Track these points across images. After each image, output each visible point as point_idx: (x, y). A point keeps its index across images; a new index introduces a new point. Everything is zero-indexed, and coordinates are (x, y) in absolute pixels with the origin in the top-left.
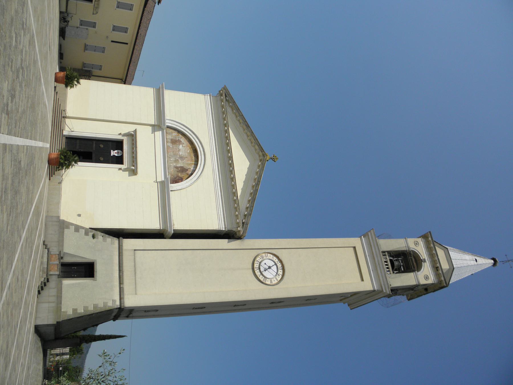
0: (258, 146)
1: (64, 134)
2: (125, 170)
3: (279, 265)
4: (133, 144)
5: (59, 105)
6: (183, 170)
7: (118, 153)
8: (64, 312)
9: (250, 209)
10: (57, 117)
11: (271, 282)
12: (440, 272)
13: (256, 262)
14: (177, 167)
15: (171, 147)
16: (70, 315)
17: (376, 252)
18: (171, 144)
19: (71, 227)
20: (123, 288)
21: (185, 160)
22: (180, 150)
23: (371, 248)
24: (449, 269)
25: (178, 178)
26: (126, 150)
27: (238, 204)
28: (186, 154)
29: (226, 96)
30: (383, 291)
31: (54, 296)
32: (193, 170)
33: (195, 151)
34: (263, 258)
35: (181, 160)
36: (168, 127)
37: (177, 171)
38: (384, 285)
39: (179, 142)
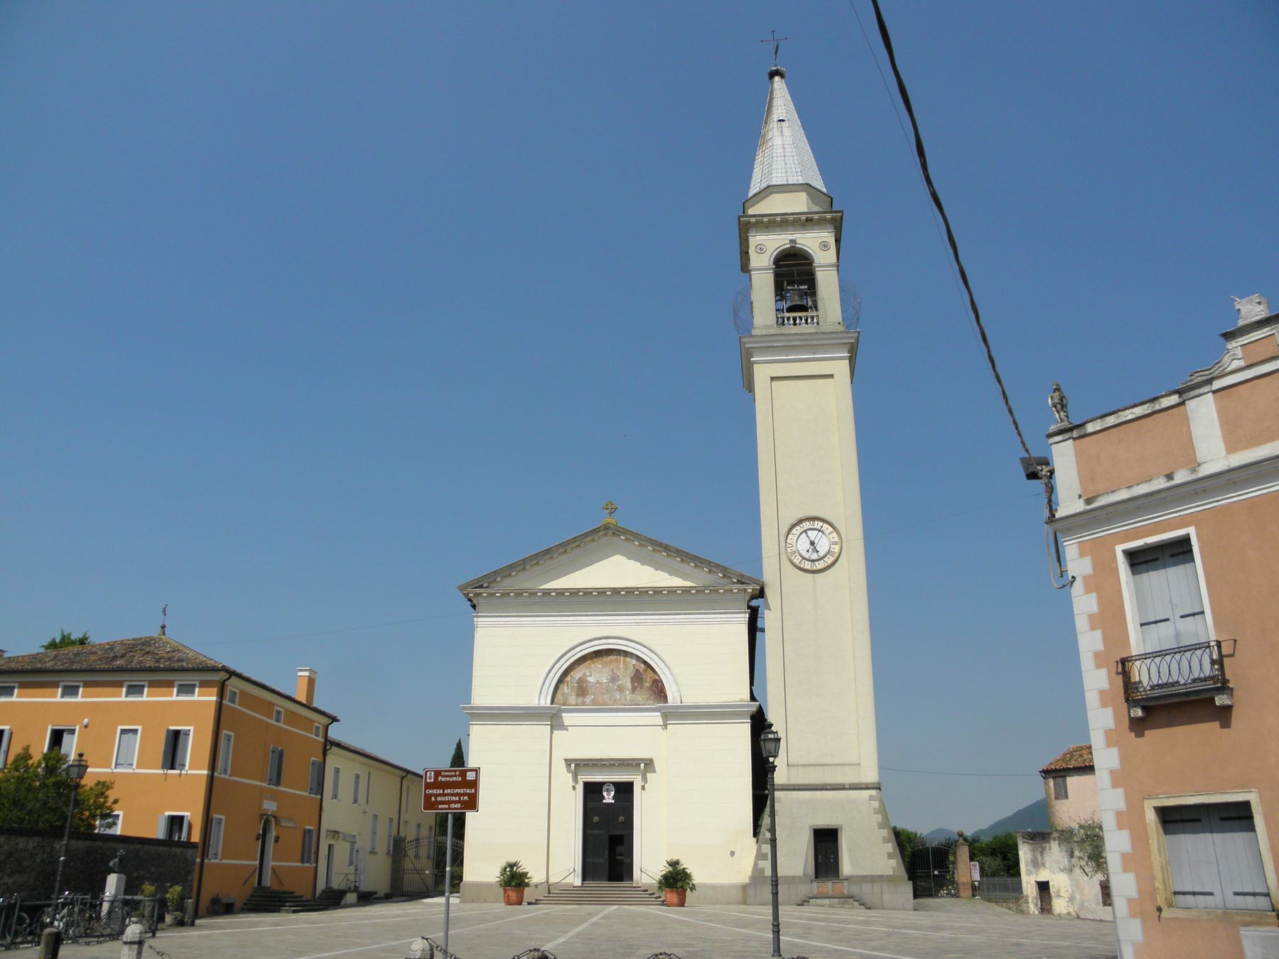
0: (587, 536)
1: (580, 884)
2: (645, 779)
3: (806, 525)
4: (593, 765)
5: (561, 892)
6: (637, 678)
7: (607, 790)
8: (894, 871)
9: (712, 567)
10: (582, 897)
11: (835, 543)
12: (816, 217)
13: (802, 566)
19: (760, 866)
20: (850, 784)
21: (618, 674)
22: (598, 681)
23: (774, 347)
24: (809, 194)
25: (653, 688)
27: (706, 587)
28: (605, 670)
29: (481, 587)
30: (851, 343)
31: (873, 886)
33: (598, 654)
36: (552, 702)
37: (641, 688)
38: (842, 338)
39: (580, 681)
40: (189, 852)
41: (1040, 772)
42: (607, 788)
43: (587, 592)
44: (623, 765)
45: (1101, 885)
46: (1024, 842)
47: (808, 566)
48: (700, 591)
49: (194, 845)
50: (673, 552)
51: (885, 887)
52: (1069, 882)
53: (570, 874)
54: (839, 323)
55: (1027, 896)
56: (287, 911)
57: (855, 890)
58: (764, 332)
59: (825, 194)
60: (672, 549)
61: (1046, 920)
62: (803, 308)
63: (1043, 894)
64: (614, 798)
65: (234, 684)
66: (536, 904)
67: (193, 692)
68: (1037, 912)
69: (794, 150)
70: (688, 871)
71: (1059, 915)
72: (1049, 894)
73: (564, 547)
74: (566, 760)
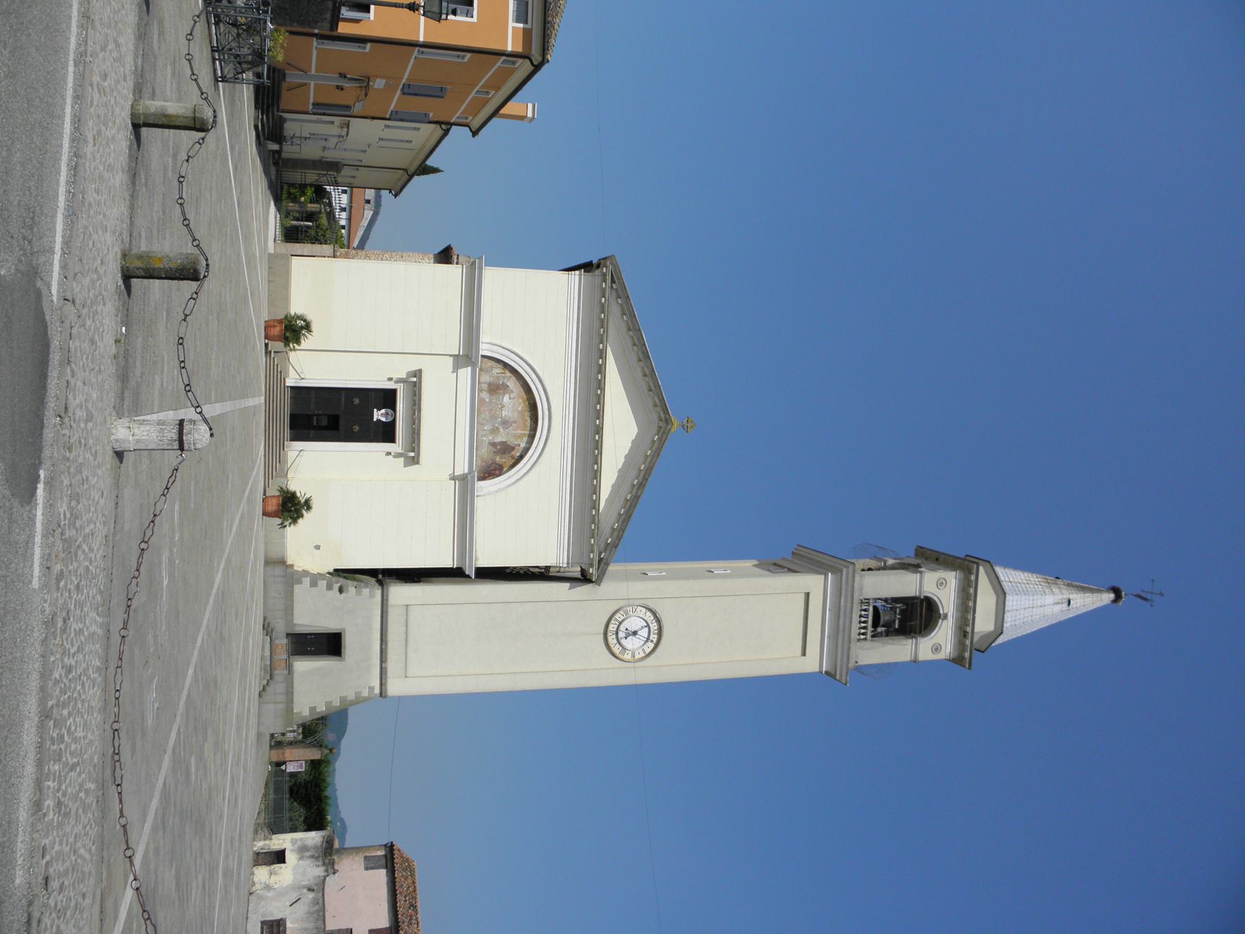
1: (287, 384)
2: (398, 455)
3: (654, 626)
4: (414, 401)
6: (505, 448)
7: (387, 414)
13: (612, 622)
14: (495, 443)
15: (487, 400)
16: (307, 716)
17: (845, 606)
18: (488, 395)
19: (304, 579)
20: (386, 668)
21: (510, 428)
24: (991, 633)
26: (401, 414)
29: (613, 281)
32: (524, 448)
33: (533, 407)
34: (627, 614)
35: (503, 428)
36: (483, 356)
37: (494, 452)
40: (327, 25)
41: (392, 842)
42: (390, 413)
43: (600, 399)
44: (414, 433)
45: (281, 919)
46: (324, 838)
47: (612, 627)
48: (593, 520)
49: (334, 26)
50: (637, 492)
51: (281, 706)
52: (285, 885)
53: (299, 374)
54: (856, 662)
55: (271, 839)
56: (256, 118)
57: (280, 673)
58: (856, 586)
59: (991, 644)
60: (640, 491)
61: (248, 858)
62: (876, 623)
63: (273, 855)
64: (379, 421)
65: (526, 67)
66: (266, 353)
67: (518, 21)
68: (255, 849)
69: (1038, 617)
70: (300, 521)
71: (252, 874)
72: (273, 863)
73: (650, 374)
74: (420, 371)
